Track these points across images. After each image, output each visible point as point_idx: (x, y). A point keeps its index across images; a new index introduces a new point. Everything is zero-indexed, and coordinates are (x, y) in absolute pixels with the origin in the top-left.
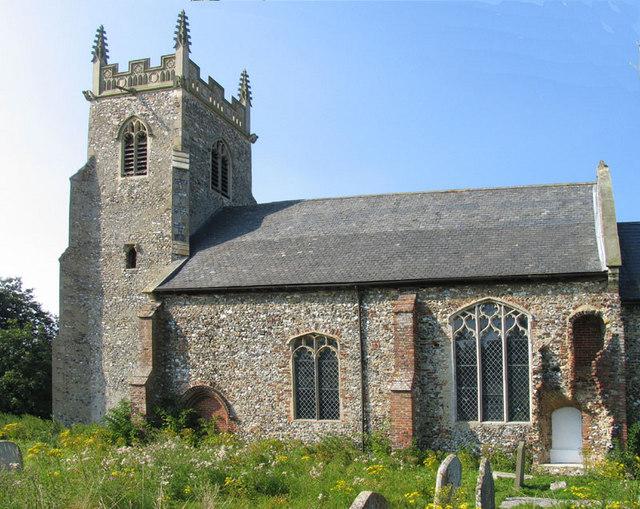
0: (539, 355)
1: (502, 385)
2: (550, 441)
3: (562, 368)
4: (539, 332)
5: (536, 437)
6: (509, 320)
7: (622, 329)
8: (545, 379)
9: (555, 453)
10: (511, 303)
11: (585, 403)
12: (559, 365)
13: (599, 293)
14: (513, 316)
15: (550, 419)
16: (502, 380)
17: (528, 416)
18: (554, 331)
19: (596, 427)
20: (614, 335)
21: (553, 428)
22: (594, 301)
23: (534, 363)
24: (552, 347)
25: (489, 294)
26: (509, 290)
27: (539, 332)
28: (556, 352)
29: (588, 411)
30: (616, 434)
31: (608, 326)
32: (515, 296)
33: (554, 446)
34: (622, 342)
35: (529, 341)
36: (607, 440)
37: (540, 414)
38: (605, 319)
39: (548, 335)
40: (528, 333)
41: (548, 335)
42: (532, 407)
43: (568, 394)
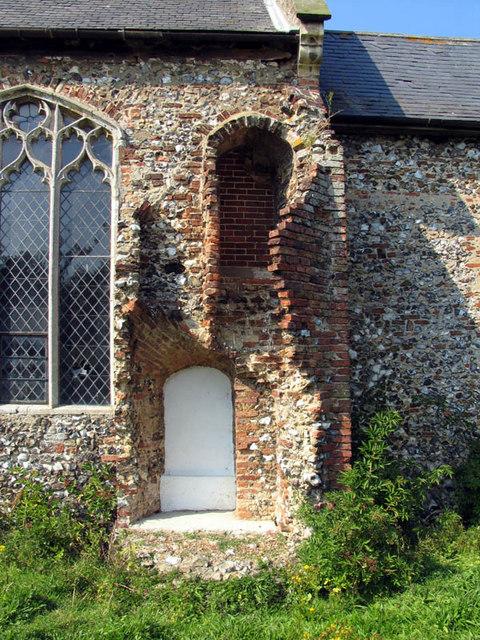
0: (134, 226)
1: (44, 307)
2: (160, 455)
3: (188, 263)
4: (137, 173)
5: (125, 448)
6: (69, 138)
7: (339, 156)
8: (146, 291)
9: (174, 488)
10: (76, 101)
11: (241, 356)
12: (181, 256)
13: (277, 87)
14: (81, 133)
15: (161, 396)
16: (45, 294)
17: (106, 391)
18: (172, 172)
19: (266, 420)
20: (319, 169)
21: (167, 418)
22: (264, 103)
23: (120, 248)
24: (167, 211)
25: (26, 77)
26: (75, 70)
27: (137, 173)
28: (176, 224)
29: (250, 379)
30: (326, 446)
31: (297, 156)
32: (87, 86)
33: (168, 465)
34: (338, 188)
35: (114, 193)
36: (304, 461)
37: (134, 385)
38: (292, 138)
39: (158, 180)
40: (112, 174)
41: (158, 180)
42: (115, 368)
43: (202, 332)
